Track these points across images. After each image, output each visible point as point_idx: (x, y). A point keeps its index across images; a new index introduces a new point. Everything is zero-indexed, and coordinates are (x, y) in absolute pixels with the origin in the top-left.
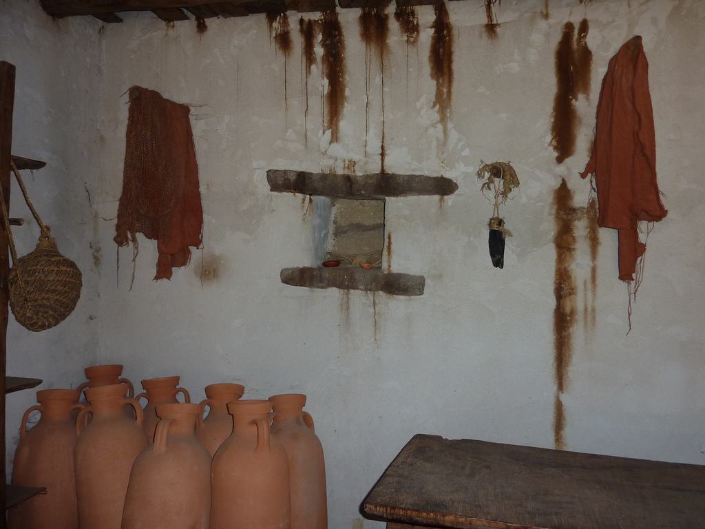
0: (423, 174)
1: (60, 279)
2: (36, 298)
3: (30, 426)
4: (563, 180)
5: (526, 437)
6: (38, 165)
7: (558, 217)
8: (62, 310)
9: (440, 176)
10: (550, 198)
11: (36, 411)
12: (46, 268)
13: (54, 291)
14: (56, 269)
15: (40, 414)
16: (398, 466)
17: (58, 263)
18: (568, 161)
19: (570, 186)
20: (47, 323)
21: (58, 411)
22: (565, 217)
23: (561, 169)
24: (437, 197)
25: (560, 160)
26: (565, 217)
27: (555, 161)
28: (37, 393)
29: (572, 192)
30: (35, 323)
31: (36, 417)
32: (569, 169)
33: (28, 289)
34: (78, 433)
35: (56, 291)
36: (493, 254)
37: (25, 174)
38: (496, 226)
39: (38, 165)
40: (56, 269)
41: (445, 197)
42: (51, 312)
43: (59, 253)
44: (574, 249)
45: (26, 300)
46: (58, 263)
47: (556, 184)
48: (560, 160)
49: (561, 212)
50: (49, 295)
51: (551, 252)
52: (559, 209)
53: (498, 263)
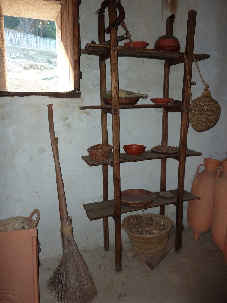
1: (210, 108)
2: (198, 117)
3: (200, 171)
5: (145, 290)
6: (207, 57)
8: (209, 123)
11: (203, 166)
12: (203, 104)
13: (206, 114)
14: (208, 104)
15: (204, 168)
16: (126, 251)
17: (210, 101)
20: (202, 128)
21: (211, 168)
28: (88, 150)
30: (197, 128)
31: (202, 168)
33: (195, 113)
34: (217, 179)
35: (207, 114)
37: (201, 63)
39: (207, 57)
40: (208, 104)
42: (204, 124)
43: (211, 97)
45: (194, 117)
46: (210, 101)
50: (204, 116)
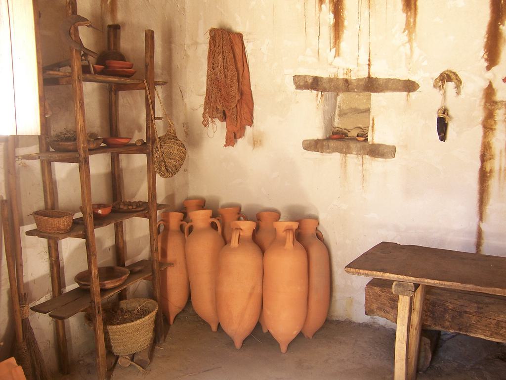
4: (490, 82)
7: (485, 107)
9: (407, 79)
10: (316, 155)
18: (494, 69)
19: (494, 86)
22: (490, 107)
23: (489, 75)
24: (405, 93)
25: (489, 68)
26: (490, 107)
27: (485, 69)
29: (496, 90)
32: (494, 75)
36: (382, 155)
38: (441, 114)
44: (495, 129)
47: (485, 85)
48: (489, 68)
49: (488, 104)
51: (479, 131)
52: (486, 102)
53: (443, 138)
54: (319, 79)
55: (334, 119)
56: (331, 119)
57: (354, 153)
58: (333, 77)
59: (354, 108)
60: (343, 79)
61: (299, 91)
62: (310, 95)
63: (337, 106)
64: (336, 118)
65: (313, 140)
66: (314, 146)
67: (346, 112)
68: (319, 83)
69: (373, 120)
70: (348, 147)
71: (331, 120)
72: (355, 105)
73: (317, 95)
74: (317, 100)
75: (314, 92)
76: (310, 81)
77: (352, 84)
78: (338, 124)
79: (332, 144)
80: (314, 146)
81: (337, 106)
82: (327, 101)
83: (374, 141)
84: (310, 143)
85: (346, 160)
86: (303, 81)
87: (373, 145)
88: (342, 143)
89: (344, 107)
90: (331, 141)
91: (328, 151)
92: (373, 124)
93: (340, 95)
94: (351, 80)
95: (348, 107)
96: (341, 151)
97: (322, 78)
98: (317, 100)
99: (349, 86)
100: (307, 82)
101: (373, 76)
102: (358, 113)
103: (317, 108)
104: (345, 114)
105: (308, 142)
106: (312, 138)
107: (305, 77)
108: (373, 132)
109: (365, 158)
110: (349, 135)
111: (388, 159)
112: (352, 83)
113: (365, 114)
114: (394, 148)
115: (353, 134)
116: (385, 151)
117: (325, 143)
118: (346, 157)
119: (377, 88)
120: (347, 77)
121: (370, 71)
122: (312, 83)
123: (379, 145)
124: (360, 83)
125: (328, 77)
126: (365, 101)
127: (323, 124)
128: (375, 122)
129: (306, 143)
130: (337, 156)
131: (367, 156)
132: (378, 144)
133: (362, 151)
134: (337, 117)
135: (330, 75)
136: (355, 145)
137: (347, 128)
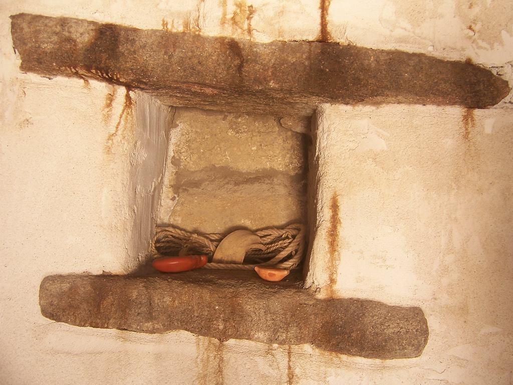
0: (423, 51)
9: (464, 59)
24: (456, 112)
41: (477, 112)
54: (123, 33)
55: (159, 198)
56: (153, 196)
57: (261, 335)
58: (181, 29)
59: (222, 168)
60: (221, 40)
61: (33, 77)
62: (81, 107)
63: (169, 161)
64: (163, 196)
65: (87, 277)
66: (84, 301)
67: (197, 177)
68: (121, 49)
69: (335, 207)
70: (233, 313)
71: (153, 200)
72: (224, 158)
73: (111, 98)
74: (107, 118)
75: (100, 88)
76: (84, 38)
77: (256, 62)
78: (174, 212)
79: (166, 296)
80: (84, 301)
81: (169, 161)
82: (144, 126)
83: (336, 287)
84: (73, 290)
85: (222, 360)
86: (55, 38)
87: (332, 302)
88: (206, 294)
89: (191, 163)
90: (160, 284)
91: (149, 325)
92: (335, 221)
93: (181, 126)
94: (252, 45)
95: (203, 164)
96: (202, 328)
97: (135, 30)
98: (107, 118)
99: (246, 68)
100: (69, 40)
101: (338, 36)
102: (236, 184)
103: (108, 150)
104: (196, 184)
105: (66, 286)
106: (79, 268)
107: (63, 22)
108: (332, 259)
109: (301, 355)
110: (218, 255)
111: (388, 362)
112: (256, 55)
113: (256, 186)
114: (416, 314)
115: (234, 250)
116: (389, 332)
117: (135, 294)
118: (220, 348)
119: (357, 81)
120: (236, 34)
121: (328, 18)
122: (92, 48)
123: (362, 306)
124: (292, 59)
125: (161, 28)
126: (254, 148)
127: (126, 213)
128: (341, 215)
129: (55, 288)
130: (184, 345)
131: (307, 348)
132: (352, 301)
133: (293, 330)
134: (166, 193)
135: (169, 21)
136: (262, 303)
137: (202, 230)
